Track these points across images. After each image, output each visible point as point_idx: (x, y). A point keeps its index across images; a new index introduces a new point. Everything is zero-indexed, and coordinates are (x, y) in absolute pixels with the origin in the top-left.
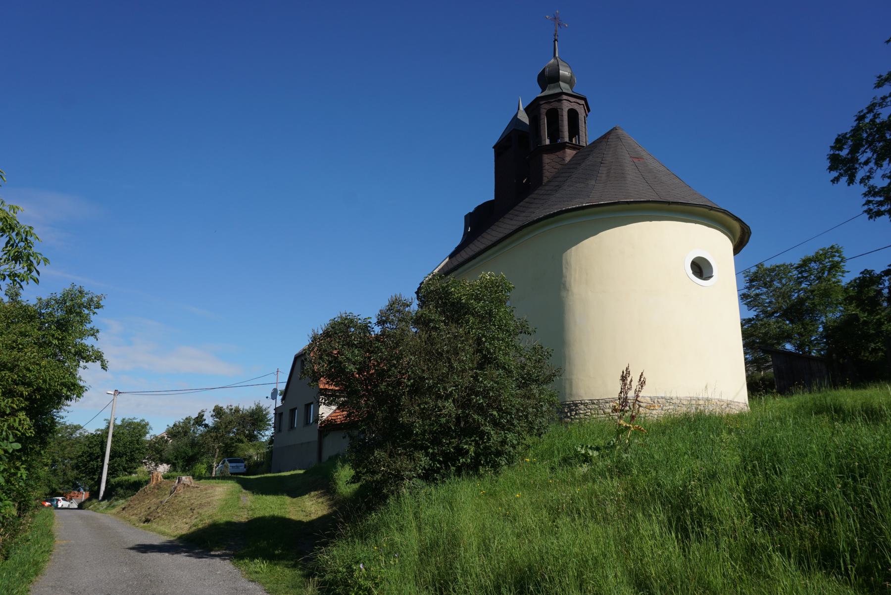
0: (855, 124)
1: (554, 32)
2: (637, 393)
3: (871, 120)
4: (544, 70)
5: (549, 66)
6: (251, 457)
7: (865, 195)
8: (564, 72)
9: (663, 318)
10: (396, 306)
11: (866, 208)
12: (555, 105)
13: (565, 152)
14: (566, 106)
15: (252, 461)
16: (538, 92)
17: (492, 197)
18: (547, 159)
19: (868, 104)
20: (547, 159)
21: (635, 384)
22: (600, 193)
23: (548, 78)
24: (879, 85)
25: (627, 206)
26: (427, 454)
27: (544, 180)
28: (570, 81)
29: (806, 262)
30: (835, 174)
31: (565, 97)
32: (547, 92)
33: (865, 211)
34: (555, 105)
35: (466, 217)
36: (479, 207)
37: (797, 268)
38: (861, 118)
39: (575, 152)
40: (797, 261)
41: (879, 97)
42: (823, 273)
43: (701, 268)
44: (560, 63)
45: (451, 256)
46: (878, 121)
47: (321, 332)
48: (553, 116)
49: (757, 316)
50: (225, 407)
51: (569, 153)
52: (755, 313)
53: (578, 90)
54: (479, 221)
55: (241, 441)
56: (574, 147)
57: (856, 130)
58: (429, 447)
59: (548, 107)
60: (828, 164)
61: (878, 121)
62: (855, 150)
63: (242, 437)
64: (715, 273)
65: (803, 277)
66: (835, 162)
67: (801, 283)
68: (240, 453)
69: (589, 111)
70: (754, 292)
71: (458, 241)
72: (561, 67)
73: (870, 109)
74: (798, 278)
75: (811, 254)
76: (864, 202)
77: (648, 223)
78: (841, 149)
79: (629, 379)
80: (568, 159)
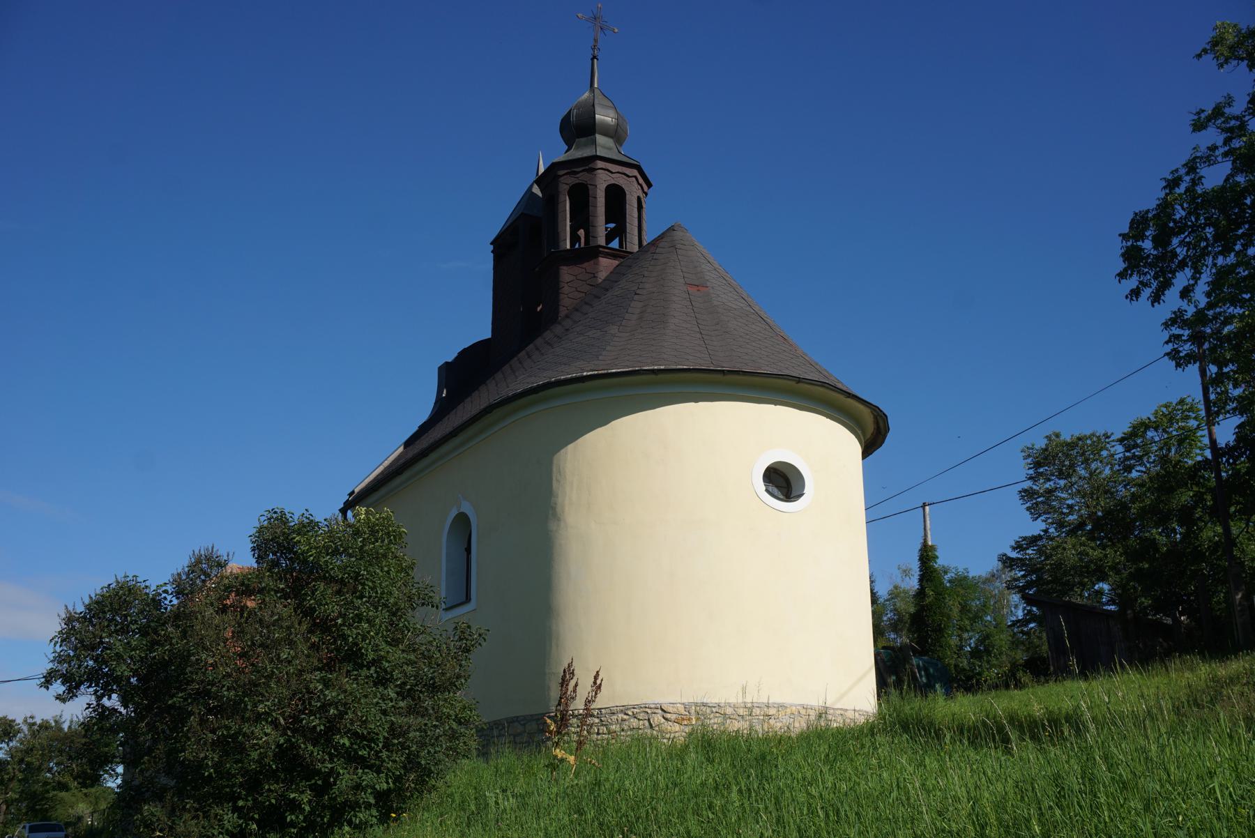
0: (1162, 195)
1: (592, 43)
2: (588, 702)
3: (1187, 190)
4: (569, 112)
5: (578, 107)
6: (80, 819)
7: (1166, 325)
8: (604, 117)
9: (736, 559)
10: (205, 565)
11: (1169, 347)
12: (583, 177)
13: (597, 264)
14: (603, 180)
15: (82, 827)
16: (560, 153)
17: (489, 335)
18: (567, 274)
19: (1185, 158)
20: (567, 274)
21: (584, 690)
22: (617, 355)
23: (578, 127)
24: (1199, 126)
25: (653, 377)
26: (236, 809)
27: (565, 312)
28: (616, 134)
29: (1140, 428)
30: (1133, 282)
31: (600, 164)
32: (576, 154)
33: (1167, 354)
34: (583, 177)
35: (440, 368)
36: (465, 350)
37: (1121, 441)
38: (1173, 183)
39: (617, 262)
40: (1120, 428)
41: (1203, 149)
42: (1169, 450)
43: (783, 482)
44: (599, 99)
45: (408, 444)
46: (1199, 190)
47: (80, 608)
48: (581, 197)
49: (1046, 531)
50: (19, 720)
51: (606, 265)
52: (1043, 526)
53: (629, 150)
54: (464, 376)
55: (63, 787)
56: (614, 254)
57: (1165, 207)
58: (239, 798)
59: (571, 180)
60: (1121, 265)
61: (1199, 190)
62: (1161, 240)
63: (67, 779)
64: (808, 489)
65: (1134, 456)
66: (1133, 259)
67: (1129, 469)
68: (61, 814)
69: (649, 185)
70: (1042, 486)
71: (424, 412)
72: (597, 109)
73: (1191, 167)
74: (1126, 459)
75: (1146, 413)
76: (1167, 338)
77: (692, 404)
78: (1142, 237)
79: (572, 683)
80: (602, 275)
